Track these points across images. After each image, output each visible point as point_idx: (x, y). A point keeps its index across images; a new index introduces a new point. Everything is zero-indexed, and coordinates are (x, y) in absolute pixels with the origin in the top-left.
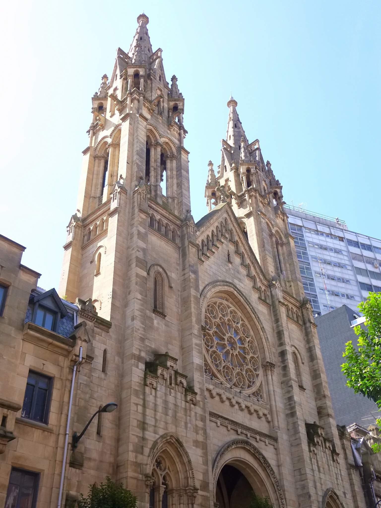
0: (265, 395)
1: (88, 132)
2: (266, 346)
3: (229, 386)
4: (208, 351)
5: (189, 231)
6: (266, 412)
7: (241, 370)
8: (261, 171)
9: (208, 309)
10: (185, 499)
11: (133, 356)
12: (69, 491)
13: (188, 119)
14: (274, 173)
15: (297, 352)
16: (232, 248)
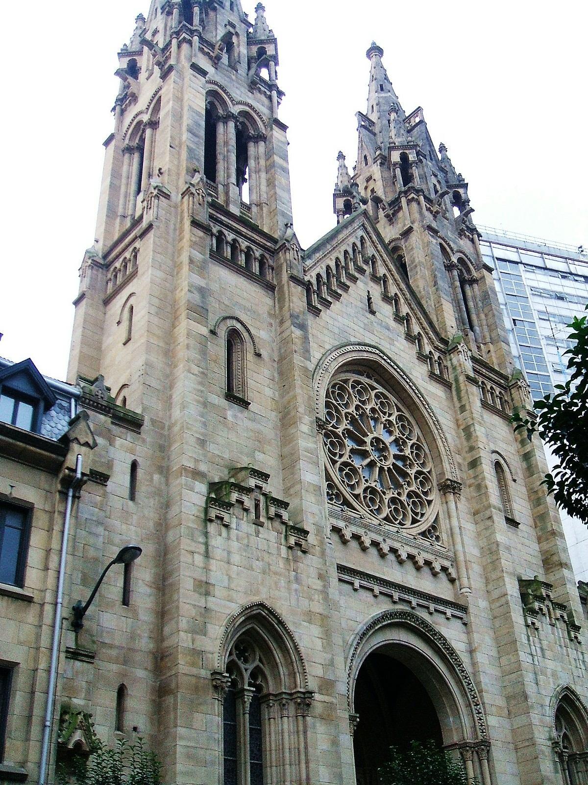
0: (444, 536)
1: (114, 109)
2: (444, 453)
3: (376, 522)
4: (334, 462)
5: (288, 257)
6: (447, 564)
7: (399, 494)
8: (428, 157)
9: (333, 392)
10: (291, 709)
11: (184, 469)
12: (70, 698)
13: (286, 75)
14: (453, 163)
15: (502, 462)
16: (376, 291)
